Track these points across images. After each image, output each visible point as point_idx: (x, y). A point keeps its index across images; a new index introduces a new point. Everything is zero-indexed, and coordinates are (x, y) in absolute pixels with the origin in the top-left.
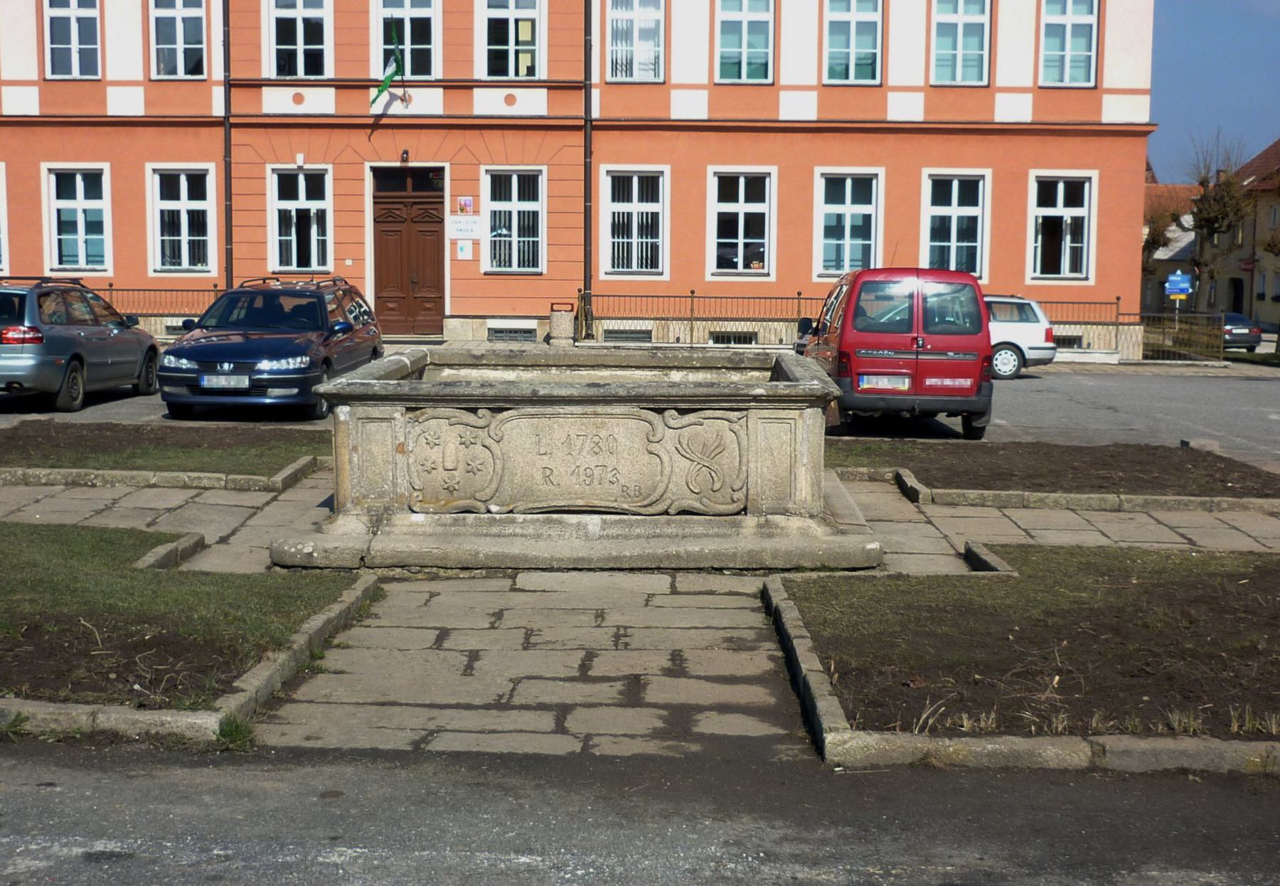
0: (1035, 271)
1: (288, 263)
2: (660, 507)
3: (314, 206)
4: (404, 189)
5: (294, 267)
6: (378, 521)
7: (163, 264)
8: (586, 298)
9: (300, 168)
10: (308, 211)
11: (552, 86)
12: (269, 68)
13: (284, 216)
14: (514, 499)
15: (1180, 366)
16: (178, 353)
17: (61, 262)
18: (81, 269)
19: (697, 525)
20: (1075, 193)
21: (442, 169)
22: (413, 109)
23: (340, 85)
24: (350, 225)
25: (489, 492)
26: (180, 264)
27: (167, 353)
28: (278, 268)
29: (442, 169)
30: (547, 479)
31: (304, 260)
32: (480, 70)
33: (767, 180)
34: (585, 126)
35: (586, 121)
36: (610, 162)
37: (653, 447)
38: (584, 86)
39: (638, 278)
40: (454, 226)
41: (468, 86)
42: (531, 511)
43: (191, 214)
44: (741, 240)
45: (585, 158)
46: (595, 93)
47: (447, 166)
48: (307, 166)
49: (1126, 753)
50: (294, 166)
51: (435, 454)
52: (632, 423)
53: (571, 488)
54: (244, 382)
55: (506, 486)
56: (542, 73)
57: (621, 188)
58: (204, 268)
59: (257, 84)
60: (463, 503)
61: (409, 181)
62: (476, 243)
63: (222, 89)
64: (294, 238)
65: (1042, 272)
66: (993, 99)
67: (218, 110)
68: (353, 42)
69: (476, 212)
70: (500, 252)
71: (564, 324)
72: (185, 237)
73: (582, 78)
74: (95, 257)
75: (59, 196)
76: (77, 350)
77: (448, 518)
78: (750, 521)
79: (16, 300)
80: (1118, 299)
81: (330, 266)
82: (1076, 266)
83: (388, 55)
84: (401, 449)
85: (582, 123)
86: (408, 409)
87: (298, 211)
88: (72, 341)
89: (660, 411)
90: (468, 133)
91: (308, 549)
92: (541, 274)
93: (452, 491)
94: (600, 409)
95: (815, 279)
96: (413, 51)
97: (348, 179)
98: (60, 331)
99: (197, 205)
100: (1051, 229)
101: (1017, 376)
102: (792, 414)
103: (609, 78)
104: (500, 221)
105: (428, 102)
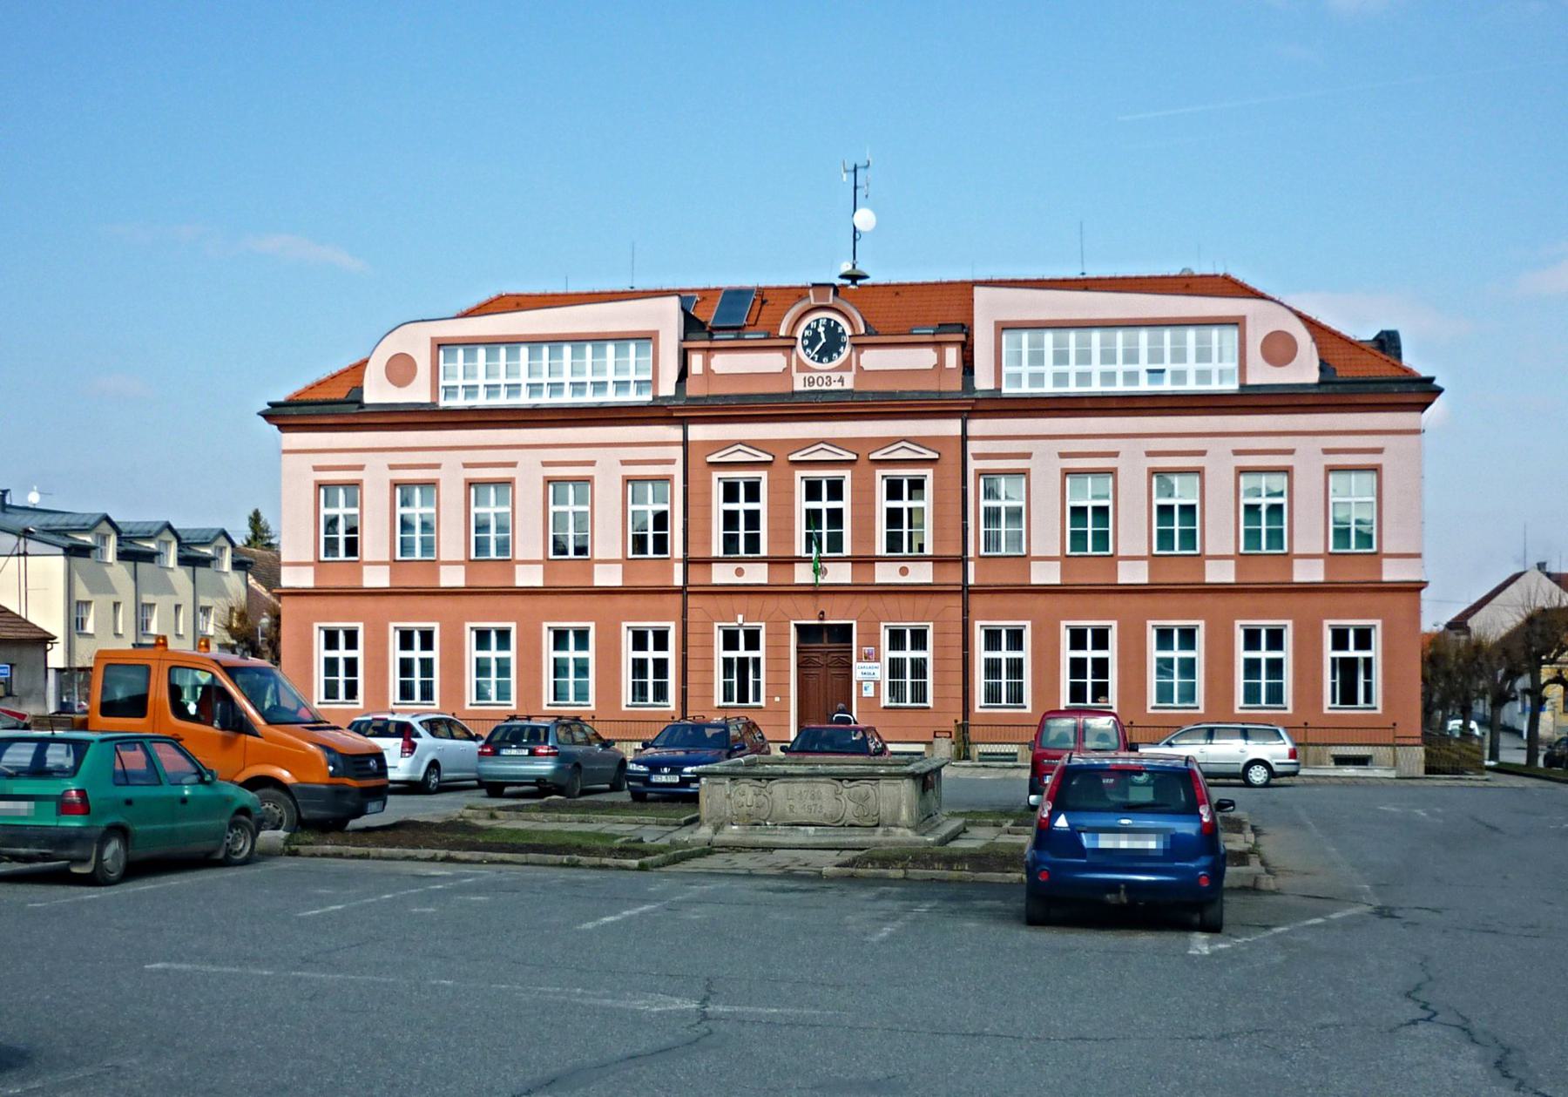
0: (1334, 701)
1: (731, 700)
2: (841, 823)
3: (751, 654)
4: (822, 642)
5: (735, 703)
6: (717, 829)
7: (634, 700)
8: (964, 728)
9: (741, 626)
10: (747, 659)
11: (937, 560)
12: (717, 549)
13: (728, 663)
14: (777, 819)
15: (1446, 779)
16: (638, 763)
17: (555, 699)
18: (570, 707)
19: (857, 831)
20: (1364, 639)
21: (851, 625)
22: (827, 580)
23: (771, 561)
24: (779, 669)
25: (766, 816)
26: (646, 701)
27: (632, 762)
28: (722, 703)
29: (851, 625)
30: (791, 811)
31: (743, 697)
32: (881, 549)
33: (1373, 633)
34: (962, 591)
35: (963, 586)
36: (982, 619)
37: (838, 797)
38: (963, 560)
39: (1004, 710)
40: (859, 670)
41: (872, 560)
42: (785, 825)
43: (422, 660)
44: (908, 680)
45: (963, 615)
46: (971, 565)
47: (854, 623)
48: (745, 624)
49: (915, 873)
50: (735, 624)
51: (743, 799)
52: (829, 785)
53: (801, 814)
54: (676, 779)
55: (774, 815)
56: (928, 551)
57: (992, 639)
58: (665, 703)
59: (708, 562)
60: (755, 821)
61: (825, 635)
62: (877, 684)
63: (681, 565)
64: (735, 680)
65: (1342, 702)
66: (1292, 562)
67: (678, 581)
68: (783, 530)
69: (877, 660)
70: (896, 691)
71: (944, 748)
72: (650, 680)
73: (959, 553)
74: (581, 694)
75: (556, 648)
76: (577, 760)
77: (748, 827)
78: (880, 830)
79: (542, 731)
80: (1395, 724)
81: (762, 703)
82: (1368, 699)
83: (809, 537)
84: (729, 797)
85: (960, 588)
86: (732, 779)
87: (739, 659)
88: (573, 755)
89: (841, 780)
90: (871, 597)
91: (686, 839)
92: (928, 708)
93: (749, 815)
94: (814, 779)
95: (1150, 711)
96: (1180, 530)
97: (778, 635)
98: (567, 749)
99: (660, 655)
100: (1347, 669)
101: (1266, 785)
102: (899, 781)
103: (982, 552)
104: (896, 668)
105: (840, 574)
